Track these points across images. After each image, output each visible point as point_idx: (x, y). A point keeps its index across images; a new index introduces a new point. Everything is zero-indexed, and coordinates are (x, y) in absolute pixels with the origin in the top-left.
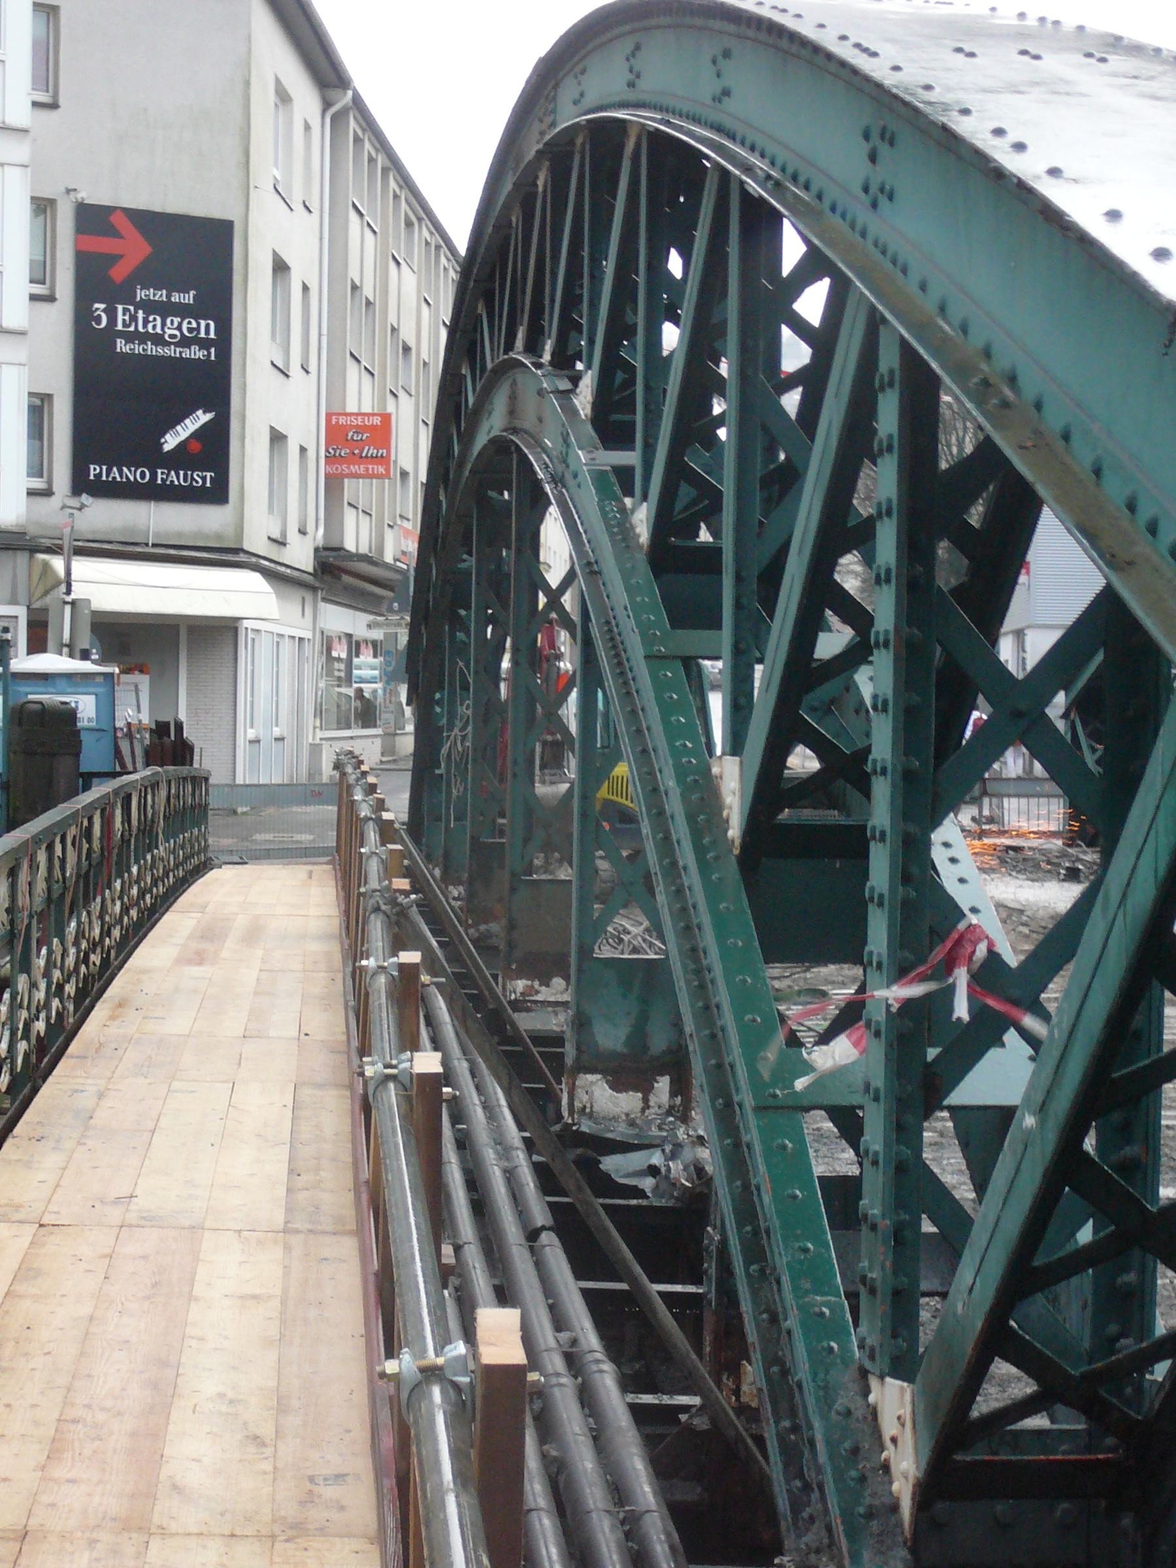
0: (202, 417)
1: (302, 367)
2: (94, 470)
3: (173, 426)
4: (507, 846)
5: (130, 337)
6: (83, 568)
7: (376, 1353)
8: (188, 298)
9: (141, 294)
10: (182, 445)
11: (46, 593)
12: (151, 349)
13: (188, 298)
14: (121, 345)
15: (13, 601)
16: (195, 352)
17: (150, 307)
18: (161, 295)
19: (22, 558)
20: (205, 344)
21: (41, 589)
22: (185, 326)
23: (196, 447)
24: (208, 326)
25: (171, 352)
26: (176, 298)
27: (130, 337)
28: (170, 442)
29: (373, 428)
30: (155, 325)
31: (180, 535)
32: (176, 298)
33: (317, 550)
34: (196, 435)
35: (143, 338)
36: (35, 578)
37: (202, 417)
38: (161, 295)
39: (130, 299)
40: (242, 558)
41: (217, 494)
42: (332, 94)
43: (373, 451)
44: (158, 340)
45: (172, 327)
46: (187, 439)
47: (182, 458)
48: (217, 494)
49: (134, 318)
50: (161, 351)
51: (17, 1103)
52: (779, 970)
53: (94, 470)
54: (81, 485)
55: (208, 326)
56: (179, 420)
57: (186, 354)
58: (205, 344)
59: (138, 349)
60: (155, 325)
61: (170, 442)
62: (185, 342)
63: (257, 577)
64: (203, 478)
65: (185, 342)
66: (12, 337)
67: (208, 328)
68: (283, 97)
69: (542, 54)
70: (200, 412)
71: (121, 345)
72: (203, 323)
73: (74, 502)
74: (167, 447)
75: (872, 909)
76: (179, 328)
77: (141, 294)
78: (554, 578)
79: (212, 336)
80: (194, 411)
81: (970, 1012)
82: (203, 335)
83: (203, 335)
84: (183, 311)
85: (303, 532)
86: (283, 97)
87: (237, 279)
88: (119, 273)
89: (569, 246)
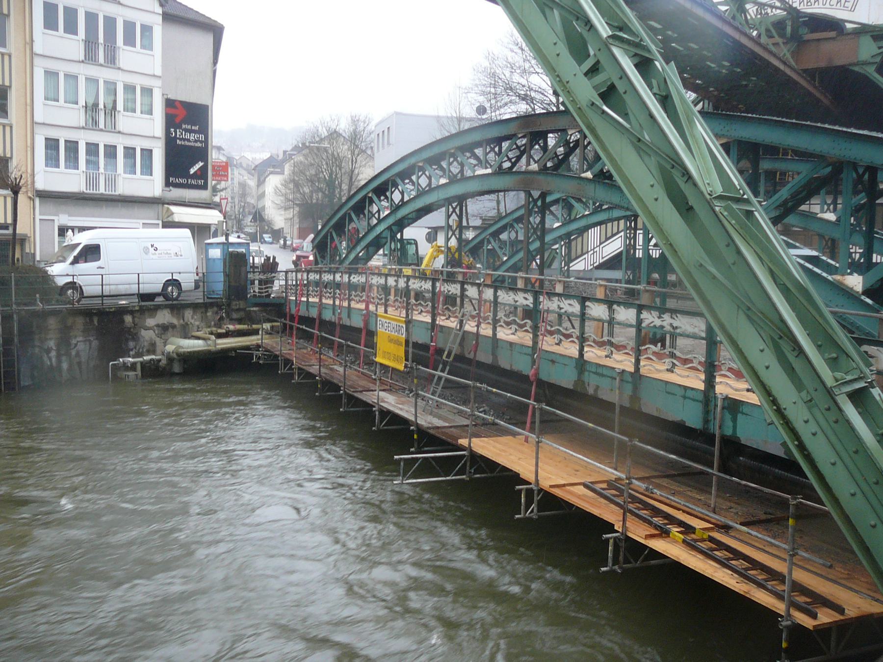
0: (201, 164)
2: (171, 179)
5: (181, 139)
6: (173, 208)
7: (600, 470)
8: (196, 128)
9: (184, 126)
10: (195, 172)
11: (168, 217)
12: (187, 143)
14: (178, 142)
15: (158, 219)
16: (199, 144)
17: (186, 130)
18: (189, 127)
19: (160, 206)
20: (201, 142)
21: (166, 216)
23: (199, 173)
25: (192, 144)
26: (193, 128)
27: (181, 139)
28: (192, 171)
29: (222, 166)
30: (188, 136)
31: (194, 199)
32: (193, 128)
35: (185, 140)
36: (165, 212)
37: (201, 164)
38: (189, 127)
39: (180, 127)
43: (223, 173)
44: (188, 140)
45: (192, 137)
47: (195, 176)
49: (182, 134)
50: (189, 144)
52: (238, 533)
53: (171, 179)
54: (168, 184)
58: (201, 142)
59: (183, 143)
60: (188, 136)
61: (192, 171)
62: (196, 141)
64: (201, 182)
65: (196, 141)
66: (143, 138)
67: (202, 137)
69: (219, 21)
71: (178, 142)
73: (168, 189)
77: (184, 126)
81: (871, 393)
84: (195, 132)
87: (210, 123)
88: (178, 120)
89: (760, 224)
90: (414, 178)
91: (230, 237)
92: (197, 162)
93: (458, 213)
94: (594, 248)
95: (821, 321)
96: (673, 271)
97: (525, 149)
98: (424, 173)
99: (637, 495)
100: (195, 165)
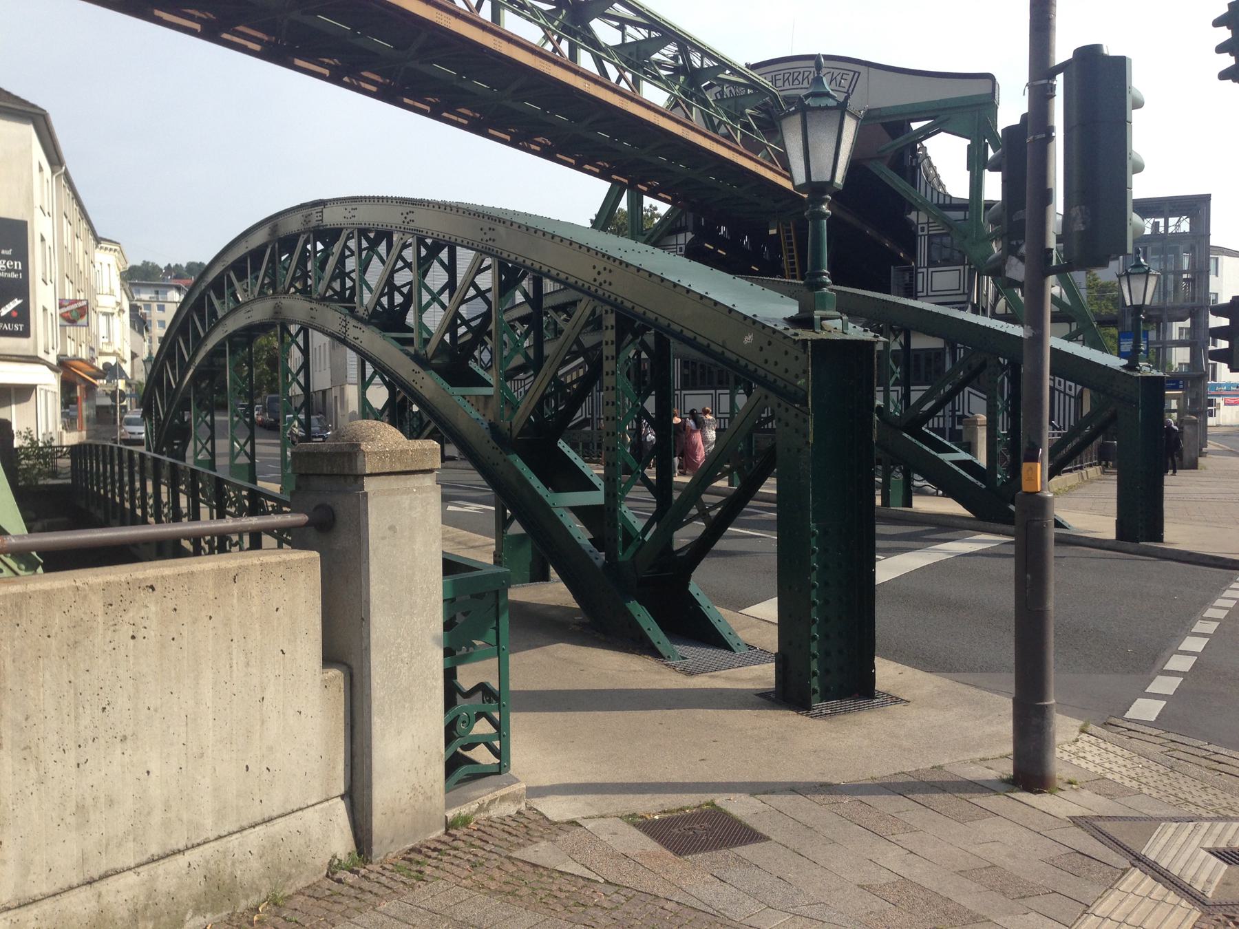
0: (17, 302)
1: (43, 280)
3: (5, 305)
4: (964, 431)
8: (9, 252)
10: (9, 314)
13: (9, 252)
16: (13, 275)
20: (17, 272)
22: (8, 264)
23: (15, 314)
24: (18, 265)
33: (58, 356)
34: (15, 309)
37: (17, 302)
40: (37, 360)
41: (26, 333)
42: (57, 168)
46: (11, 311)
47: (8, 319)
48: (26, 333)
51: (956, 468)
55: (18, 265)
56: (8, 302)
57: (9, 275)
58: (17, 272)
62: (8, 271)
63: (45, 367)
64: (18, 327)
67: (18, 265)
68: (41, 169)
70: (16, 300)
72: (16, 263)
74: (3, 314)
75: (181, 495)
76: (6, 264)
78: (294, 371)
79: (20, 268)
80: (13, 299)
82: (16, 267)
83: (16, 267)
85: (53, 348)
86: (41, 169)
90: (476, 353)
91: (1175, 486)
92: (11, 300)
93: (301, 344)
94: (518, 389)
95: (28, 109)
96: (277, 372)
97: (410, 291)
98: (486, 347)
99: (1147, 558)
100: (8, 303)
